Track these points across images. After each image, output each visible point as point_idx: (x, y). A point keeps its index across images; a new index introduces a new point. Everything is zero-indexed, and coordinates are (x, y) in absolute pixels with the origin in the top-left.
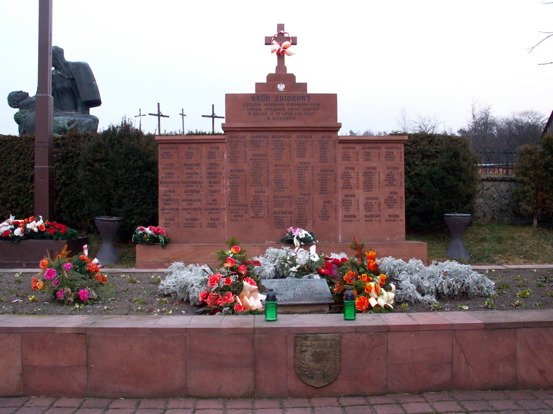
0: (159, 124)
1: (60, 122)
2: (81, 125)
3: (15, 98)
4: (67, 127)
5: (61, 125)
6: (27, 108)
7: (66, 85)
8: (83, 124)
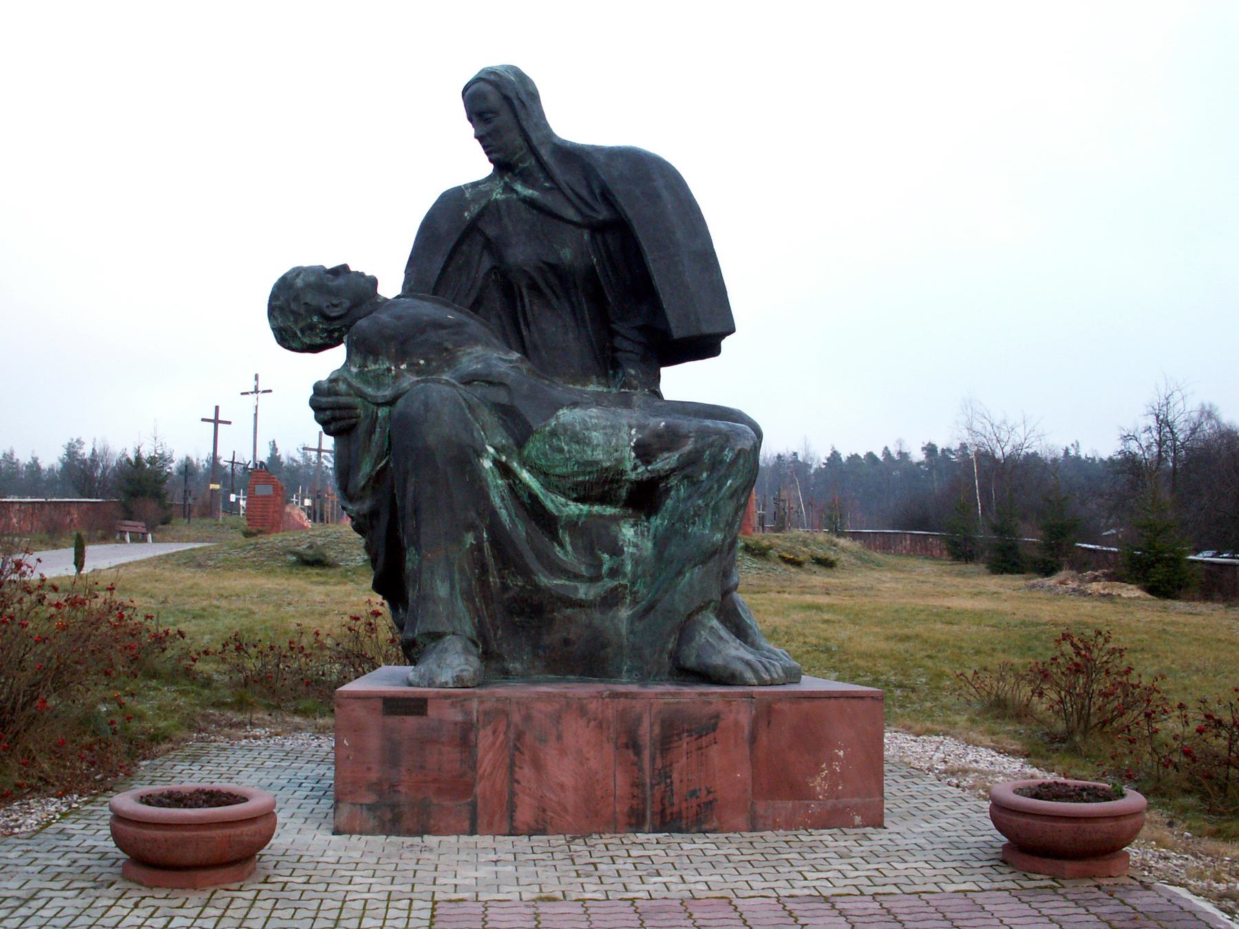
0: (256, 415)
1: (596, 436)
2: (716, 463)
3: (322, 302)
4: (628, 466)
5: (599, 455)
6: (401, 356)
7: (567, 254)
8: (728, 455)
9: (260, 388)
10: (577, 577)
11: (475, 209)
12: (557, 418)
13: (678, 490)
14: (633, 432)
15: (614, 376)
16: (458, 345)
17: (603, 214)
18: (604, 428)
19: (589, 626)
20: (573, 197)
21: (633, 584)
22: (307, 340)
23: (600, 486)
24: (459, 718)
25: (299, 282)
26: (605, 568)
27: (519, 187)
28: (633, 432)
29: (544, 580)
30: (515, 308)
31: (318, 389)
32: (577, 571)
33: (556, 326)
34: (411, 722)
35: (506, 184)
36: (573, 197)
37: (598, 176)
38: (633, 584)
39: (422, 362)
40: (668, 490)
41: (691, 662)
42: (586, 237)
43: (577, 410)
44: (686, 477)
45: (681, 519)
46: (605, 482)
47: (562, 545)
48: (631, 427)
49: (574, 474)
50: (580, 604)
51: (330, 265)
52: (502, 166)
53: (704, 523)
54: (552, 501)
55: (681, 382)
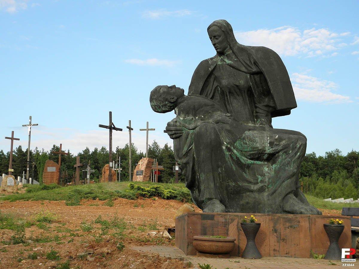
0: (30, 135)
4: (267, 149)
5: (258, 145)
7: (242, 82)
9: (32, 123)
10: (250, 182)
11: (212, 67)
12: (245, 134)
13: (282, 156)
14: (268, 138)
15: (257, 120)
16: (213, 111)
17: (254, 69)
18: (259, 137)
19: (255, 198)
20: (244, 64)
21: (268, 185)
22: (164, 109)
23: (258, 156)
24: (224, 221)
25: (161, 91)
26: (259, 180)
27: (226, 60)
28: (268, 138)
29: (240, 184)
30: (224, 99)
31: (169, 124)
32: (251, 181)
33: (238, 104)
34: (209, 221)
35: (222, 59)
36: (244, 64)
37: (253, 58)
38: (268, 185)
39: (203, 116)
40: (278, 156)
41: (288, 208)
42: (248, 76)
43: (250, 131)
44: (285, 152)
45: (283, 165)
46: (259, 154)
47: (245, 173)
48: (268, 137)
49: (250, 151)
50: (252, 191)
51: (169, 85)
52: (220, 53)
53: (290, 166)
54: (243, 160)
55: (278, 123)
